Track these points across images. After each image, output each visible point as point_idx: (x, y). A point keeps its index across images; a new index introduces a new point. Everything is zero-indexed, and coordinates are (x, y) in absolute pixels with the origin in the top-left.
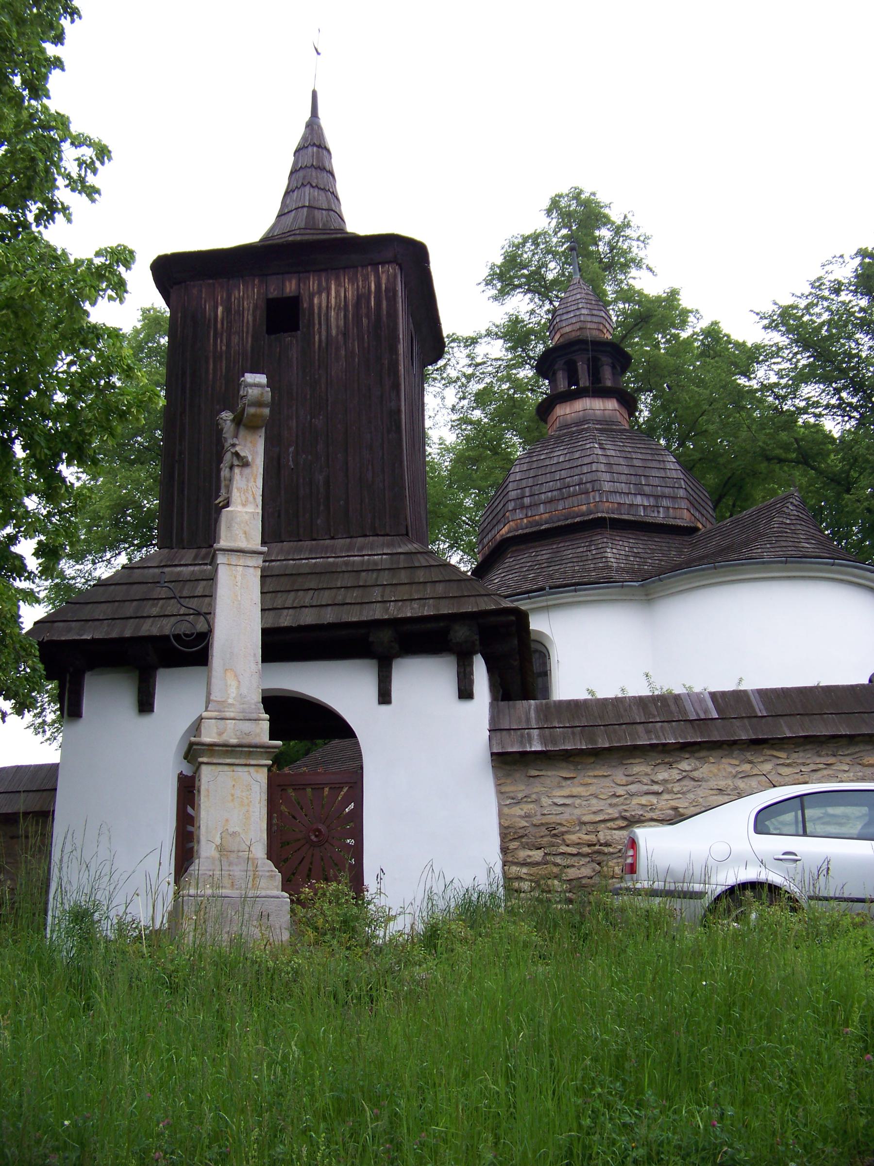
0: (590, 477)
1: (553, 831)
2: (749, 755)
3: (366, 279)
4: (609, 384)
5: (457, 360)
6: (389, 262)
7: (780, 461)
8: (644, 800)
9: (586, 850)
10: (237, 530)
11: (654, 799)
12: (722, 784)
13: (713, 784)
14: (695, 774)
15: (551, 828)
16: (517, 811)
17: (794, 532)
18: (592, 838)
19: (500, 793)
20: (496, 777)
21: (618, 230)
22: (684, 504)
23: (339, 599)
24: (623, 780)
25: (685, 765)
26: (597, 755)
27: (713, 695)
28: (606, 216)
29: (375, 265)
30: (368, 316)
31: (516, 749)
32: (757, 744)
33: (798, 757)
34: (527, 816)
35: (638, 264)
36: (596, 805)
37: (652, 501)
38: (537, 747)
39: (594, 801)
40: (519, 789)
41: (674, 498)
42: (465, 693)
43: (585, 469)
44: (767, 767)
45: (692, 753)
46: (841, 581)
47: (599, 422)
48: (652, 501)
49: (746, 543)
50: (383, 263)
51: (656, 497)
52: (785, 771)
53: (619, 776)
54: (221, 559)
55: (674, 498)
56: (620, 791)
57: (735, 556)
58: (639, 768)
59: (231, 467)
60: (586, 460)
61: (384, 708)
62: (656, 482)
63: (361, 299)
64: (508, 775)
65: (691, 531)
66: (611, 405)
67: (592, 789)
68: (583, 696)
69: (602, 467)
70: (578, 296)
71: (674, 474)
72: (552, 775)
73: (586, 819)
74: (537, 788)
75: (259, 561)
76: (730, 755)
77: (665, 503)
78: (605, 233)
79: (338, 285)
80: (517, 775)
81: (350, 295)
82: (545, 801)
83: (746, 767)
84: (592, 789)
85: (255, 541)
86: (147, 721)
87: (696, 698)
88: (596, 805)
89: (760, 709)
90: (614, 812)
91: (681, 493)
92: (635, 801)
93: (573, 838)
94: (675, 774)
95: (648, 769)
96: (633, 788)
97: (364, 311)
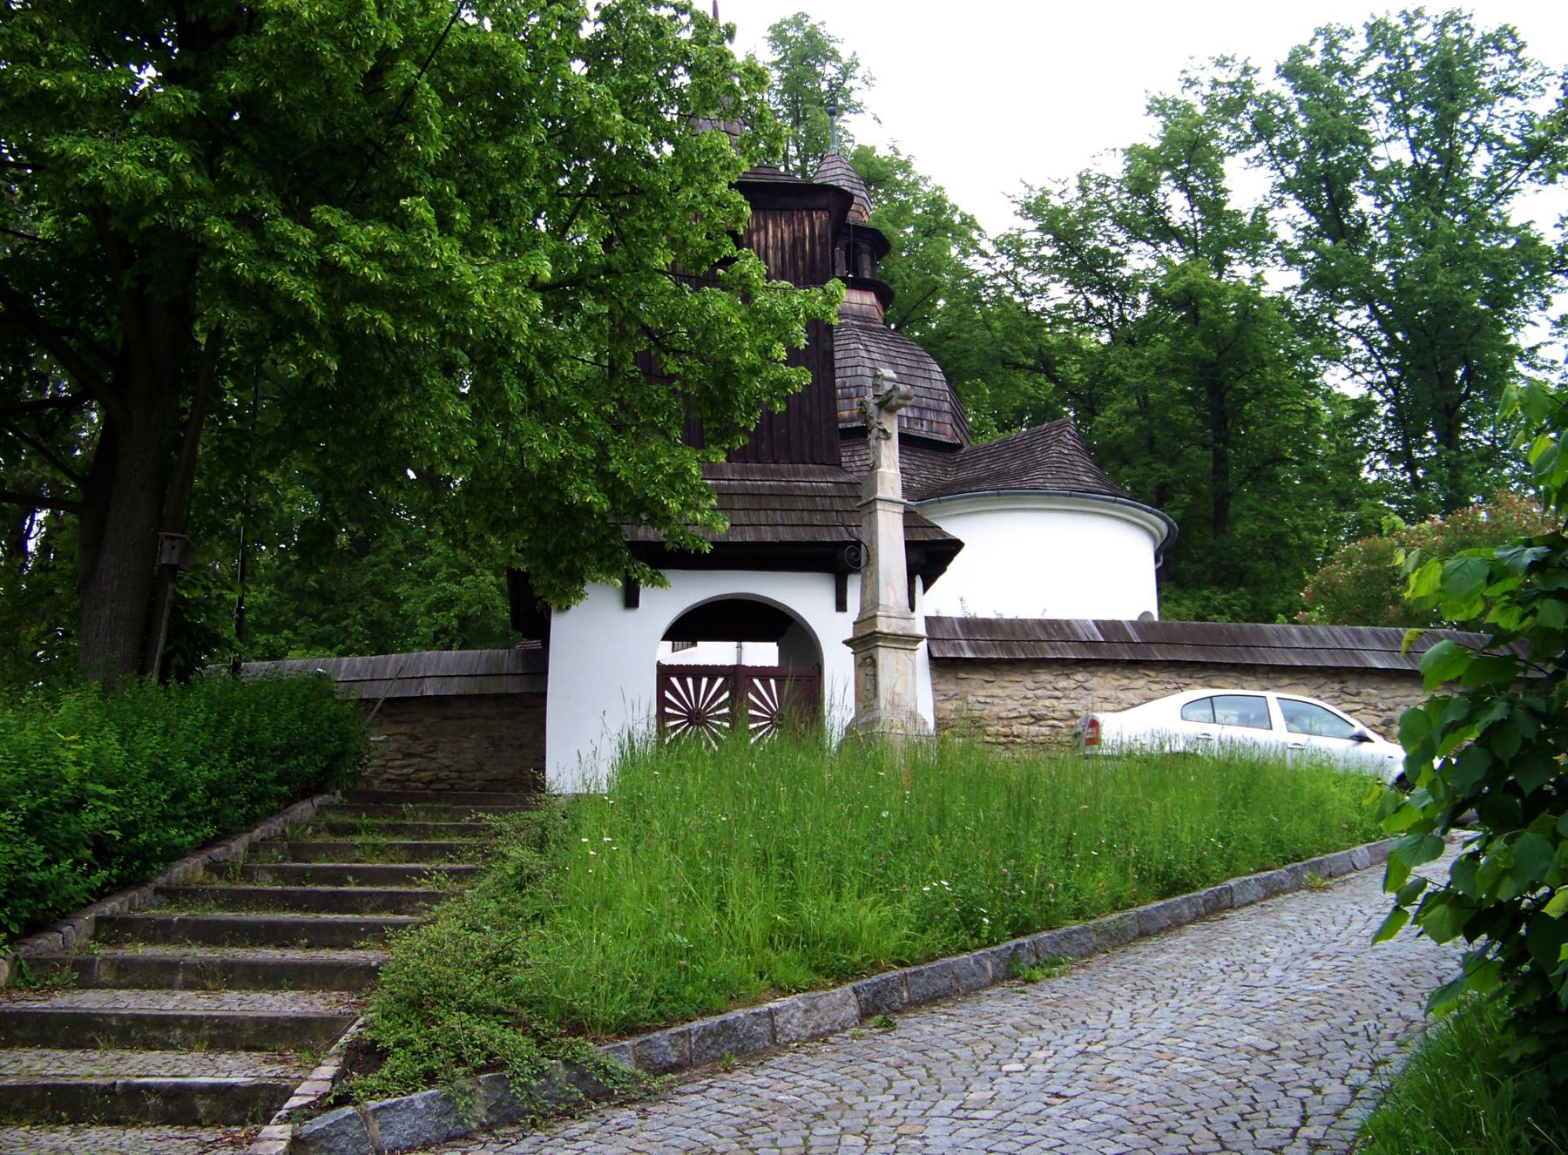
0: (854, 381)
1: (977, 724)
2: (1127, 673)
3: (802, 223)
4: (867, 275)
5: (844, 292)
6: (822, 210)
7: (1018, 366)
8: (1048, 702)
9: (1002, 739)
10: (887, 486)
11: (1055, 702)
12: (1107, 694)
13: (1100, 693)
14: (1087, 685)
15: (974, 720)
16: (949, 706)
17: (1072, 463)
18: (1007, 730)
19: (935, 690)
20: (933, 678)
21: (846, 72)
22: (948, 419)
23: (806, 520)
24: (1030, 684)
25: (1079, 677)
26: (1013, 665)
27: (1096, 622)
28: (834, 52)
29: (810, 210)
30: (803, 259)
31: (952, 655)
32: (1134, 665)
33: (1164, 677)
34: (956, 710)
35: (856, 109)
36: (1011, 704)
37: (916, 413)
38: (969, 655)
39: (1009, 701)
40: (950, 688)
41: (938, 411)
42: (841, 606)
43: (849, 372)
44: (1141, 682)
45: (1085, 667)
46: (1127, 521)
47: (856, 317)
48: (916, 413)
49: (1025, 470)
50: (817, 210)
51: (921, 409)
52: (1154, 687)
53: (1028, 682)
54: (879, 506)
55: (938, 411)
56: (1030, 694)
57: (1017, 484)
58: (1045, 676)
59: (878, 438)
60: (851, 362)
61: (841, 614)
62: (921, 392)
63: (797, 241)
64: (941, 676)
65: (954, 448)
66: (869, 299)
67: (1008, 692)
68: (992, 616)
69: (868, 372)
70: (839, 171)
71: (939, 386)
72: (977, 678)
73: (1003, 715)
74: (965, 687)
75: (901, 509)
76: (1113, 672)
77: (930, 415)
78: (830, 70)
79: (775, 225)
80: (949, 677)
81: (786, 235)
82: (971, 699)
83: (1125, 682)
84: (1008, 692)
85: (897, 495)
86: (631, 615)
87: (1083, 623)
88: (1011, 704)
89: (1135, 638)
90: (1024, 711)
91: (946, 406)
92: (1041, 703)
93: (991, 730)
94: (1071, 683)
95: (1051, 678)
96: (1039, 692)
97: (799, 254)
